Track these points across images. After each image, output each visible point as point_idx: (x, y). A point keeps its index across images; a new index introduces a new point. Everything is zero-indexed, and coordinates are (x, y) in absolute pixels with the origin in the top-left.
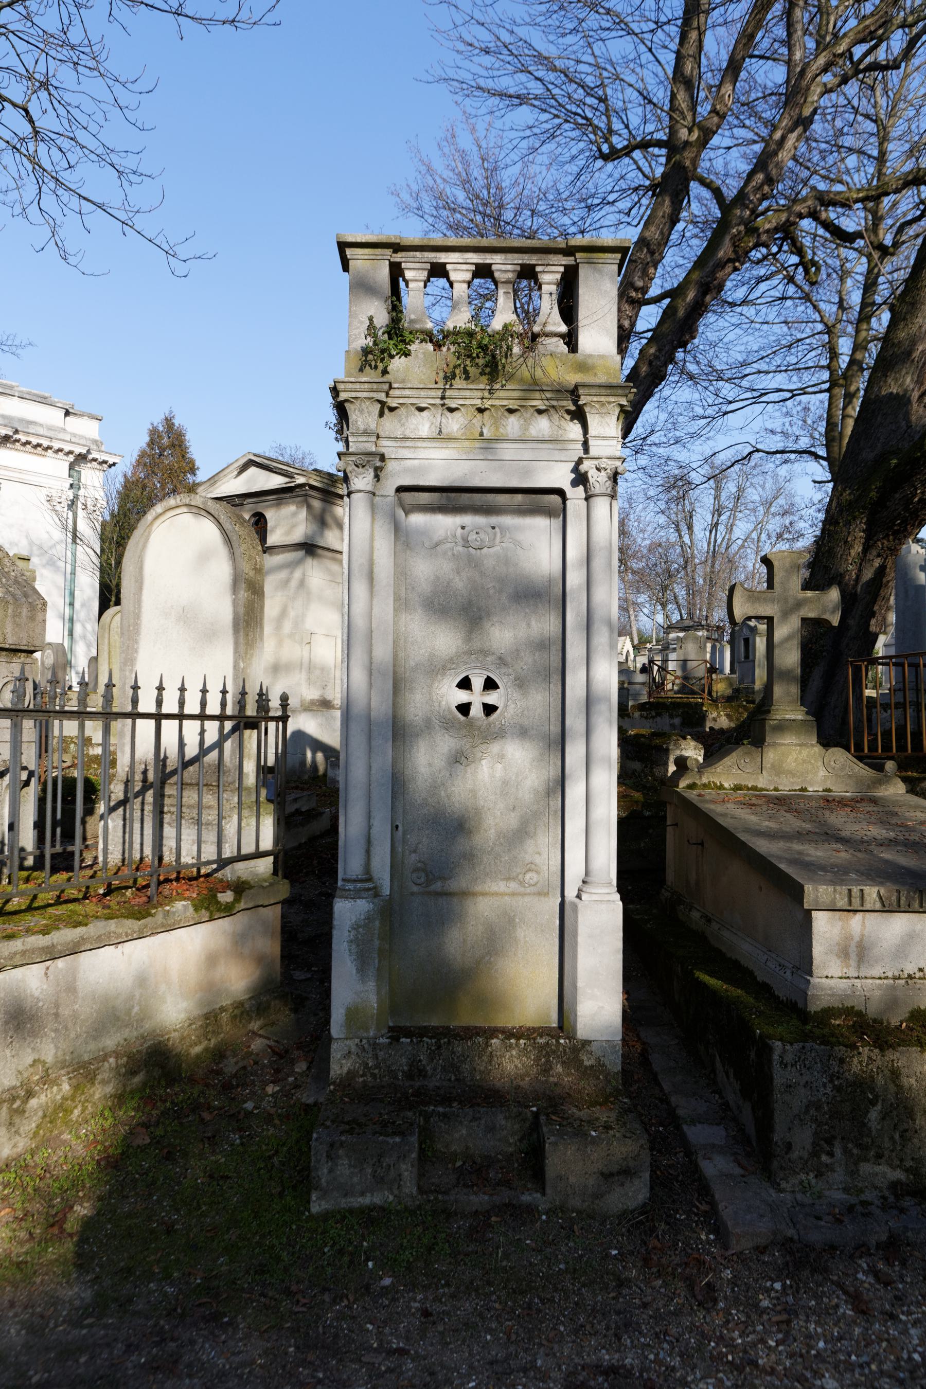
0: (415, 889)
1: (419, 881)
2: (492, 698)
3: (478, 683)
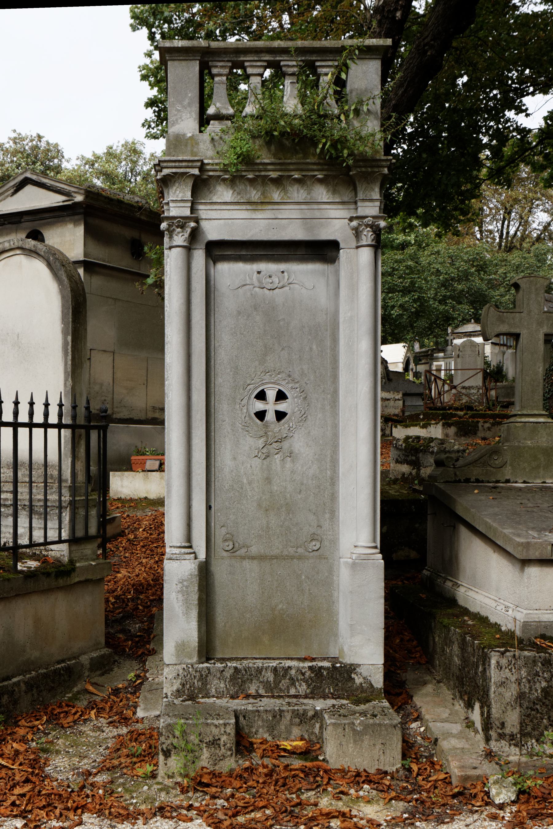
0: (225, 554)
1: (227, 549)
2: (282, 407)
3: (271, 395)
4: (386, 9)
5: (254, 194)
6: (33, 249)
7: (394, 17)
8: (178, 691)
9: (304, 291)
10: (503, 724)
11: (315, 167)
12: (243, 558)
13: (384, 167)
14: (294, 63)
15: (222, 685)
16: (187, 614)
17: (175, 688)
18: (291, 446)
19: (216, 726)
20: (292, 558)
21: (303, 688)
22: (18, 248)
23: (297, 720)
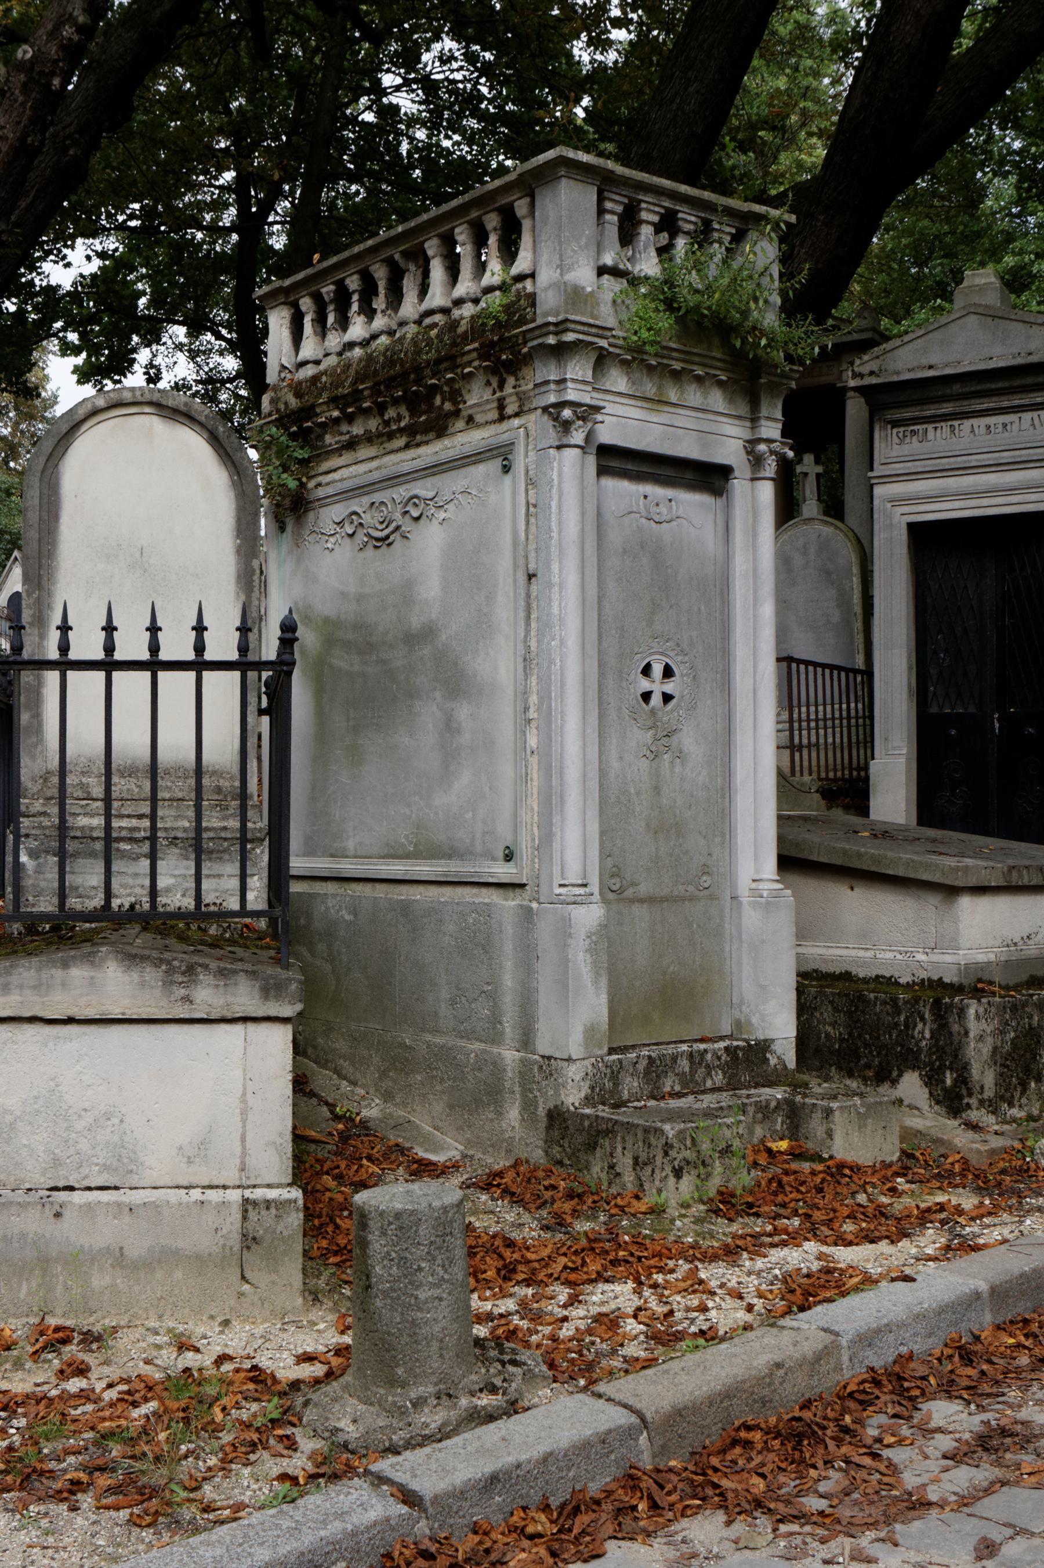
4: (37, 69)
5: (649, 388)
6: (183, 408)
7: (50, 84)
8: (586, 1098)
9: (692, 529)
10: (982, 1087)
11: (719, 364)
12: (632, 901)
13: (792, 379)
14: (693, 219)
15: (636, 1084)
16: (596, 982)
17: (583, 1095)
18: (679, 743)
19: (728, 1126)
20: (682, 899)
21: (719, 1078)
22: (150, 403)
23: (760, 1115)
